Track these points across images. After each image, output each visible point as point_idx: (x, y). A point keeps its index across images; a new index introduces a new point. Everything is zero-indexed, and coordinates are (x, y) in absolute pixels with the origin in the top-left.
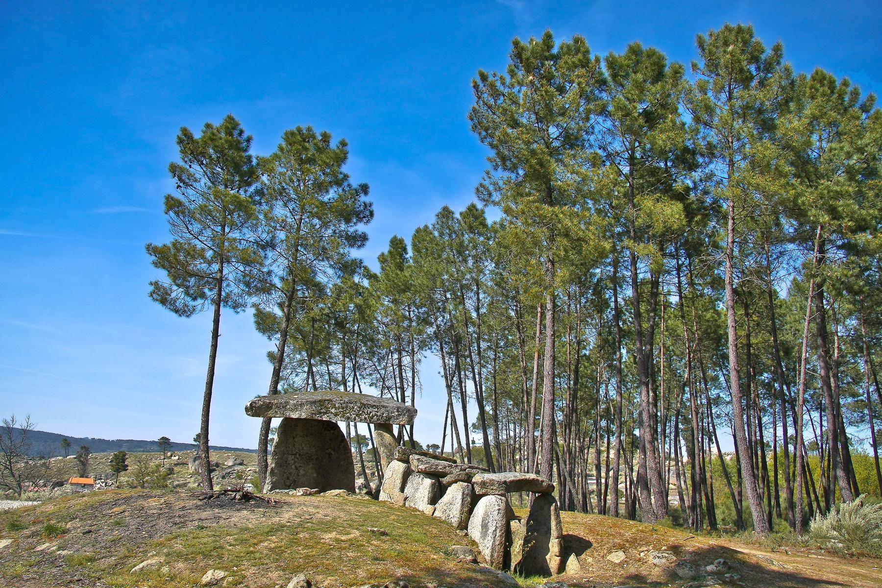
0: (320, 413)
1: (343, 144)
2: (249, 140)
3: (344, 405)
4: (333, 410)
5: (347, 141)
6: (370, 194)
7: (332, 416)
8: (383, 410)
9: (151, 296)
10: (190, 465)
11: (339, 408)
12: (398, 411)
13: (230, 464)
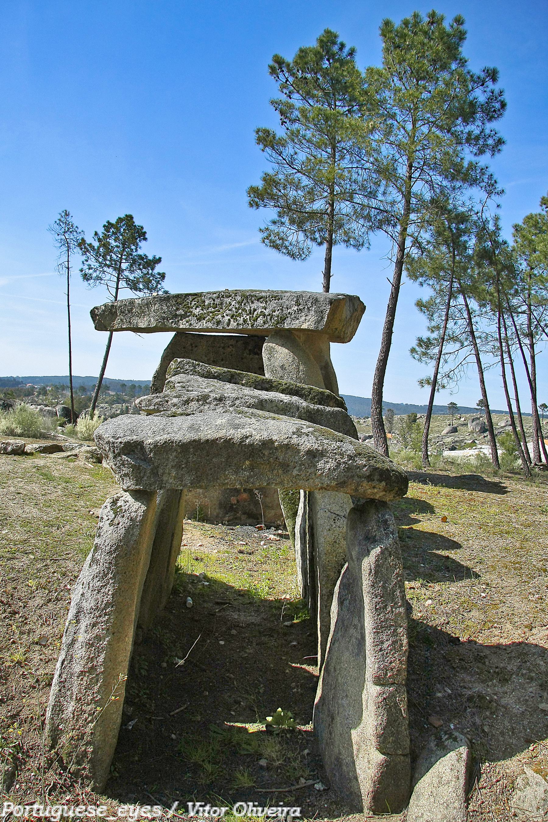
0: (176, 316)
1: (459, 21)
2: (352, 53)
3: (217, 301)
4: (197, 311)
5: (465, 17)
6: (500, 80)
7: (193, 320)
8: (273, 304)
9: (264, 242)
10: (469, 425)
11: (209, 306)
12: (298, 304)
13: (503, 425)
